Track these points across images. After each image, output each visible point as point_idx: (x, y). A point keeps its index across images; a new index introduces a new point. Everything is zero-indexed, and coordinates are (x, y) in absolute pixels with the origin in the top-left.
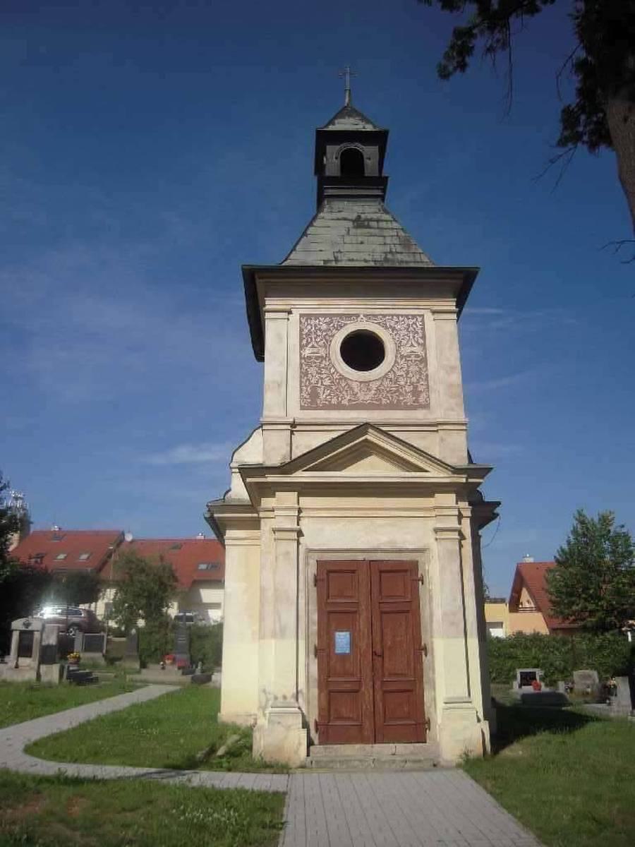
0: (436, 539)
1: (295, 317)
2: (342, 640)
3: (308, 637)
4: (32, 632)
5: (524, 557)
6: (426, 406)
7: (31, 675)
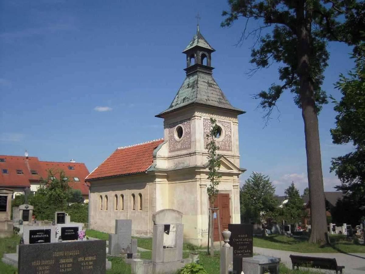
0: (234, 188)
1: (202, 119)
4: (29, 210)
5: (71, 160)
6: (231, 151)
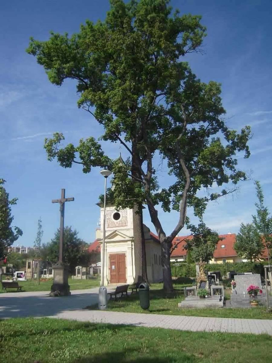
2: (113, 267)
3: (108, 267)
4: (80, 269)
7: (80, 278)
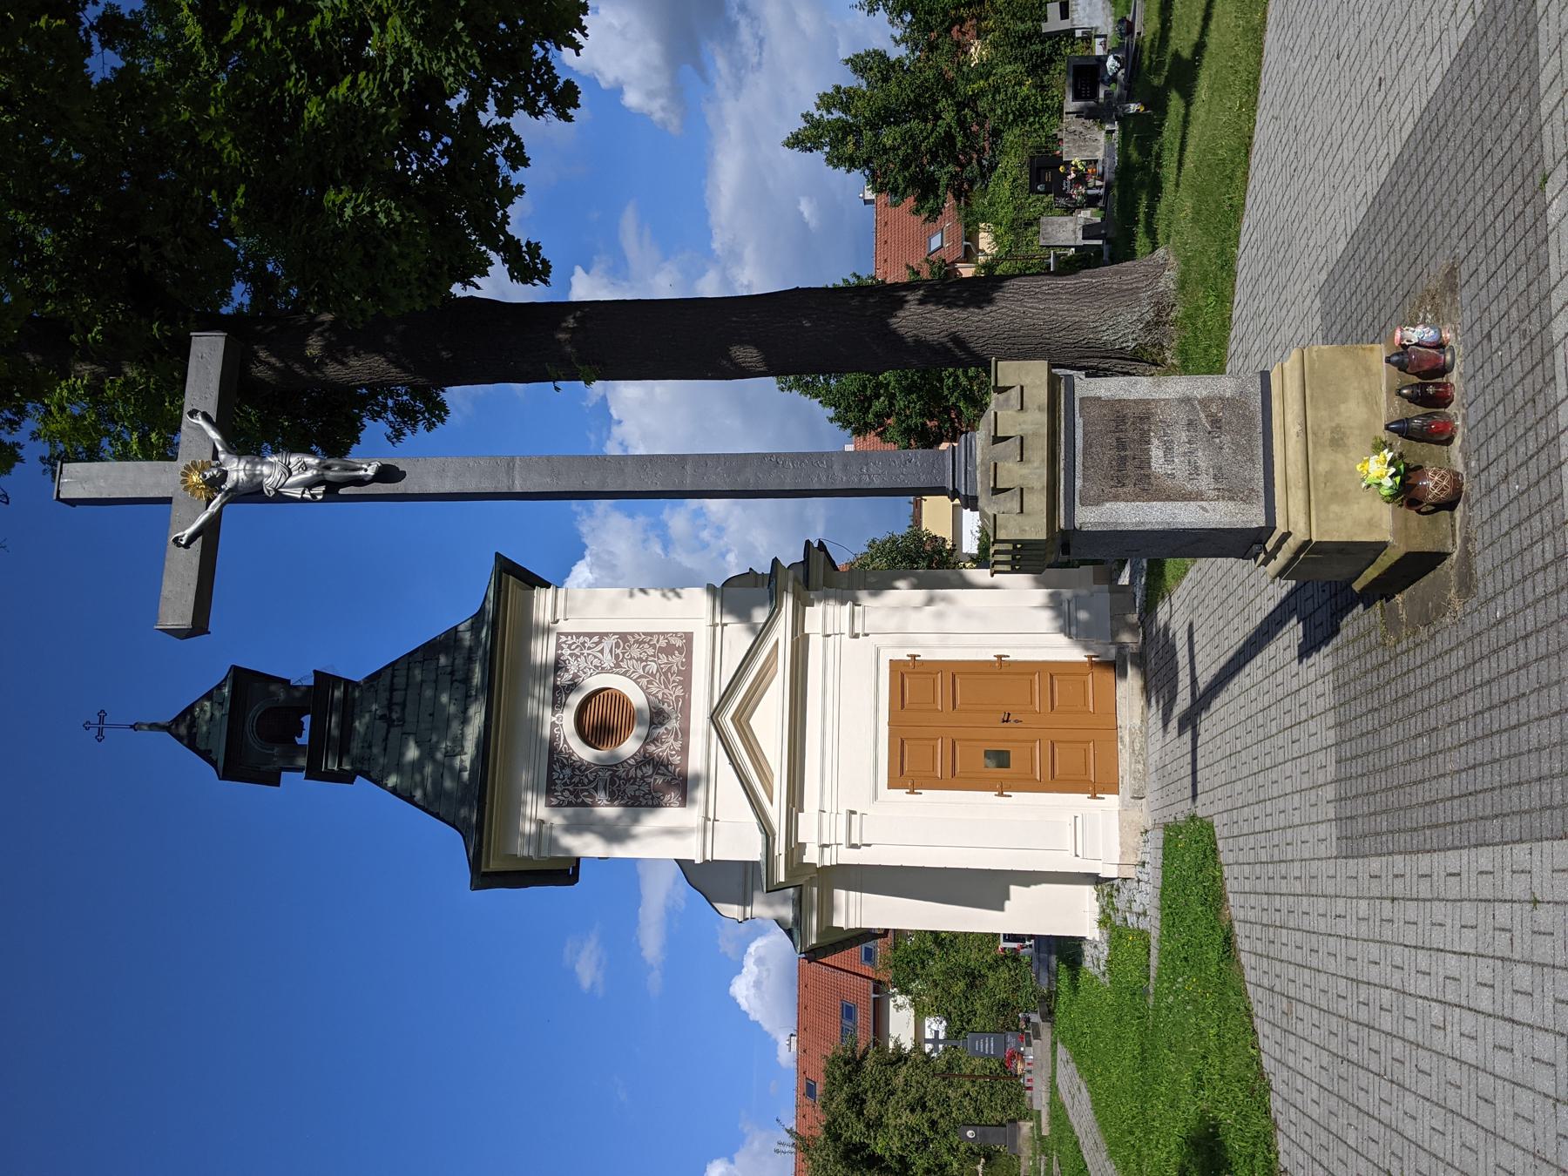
6: (688, 637)
